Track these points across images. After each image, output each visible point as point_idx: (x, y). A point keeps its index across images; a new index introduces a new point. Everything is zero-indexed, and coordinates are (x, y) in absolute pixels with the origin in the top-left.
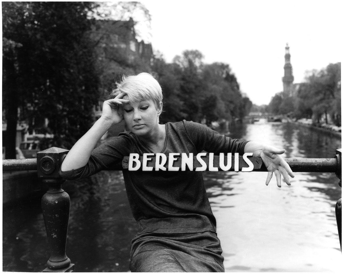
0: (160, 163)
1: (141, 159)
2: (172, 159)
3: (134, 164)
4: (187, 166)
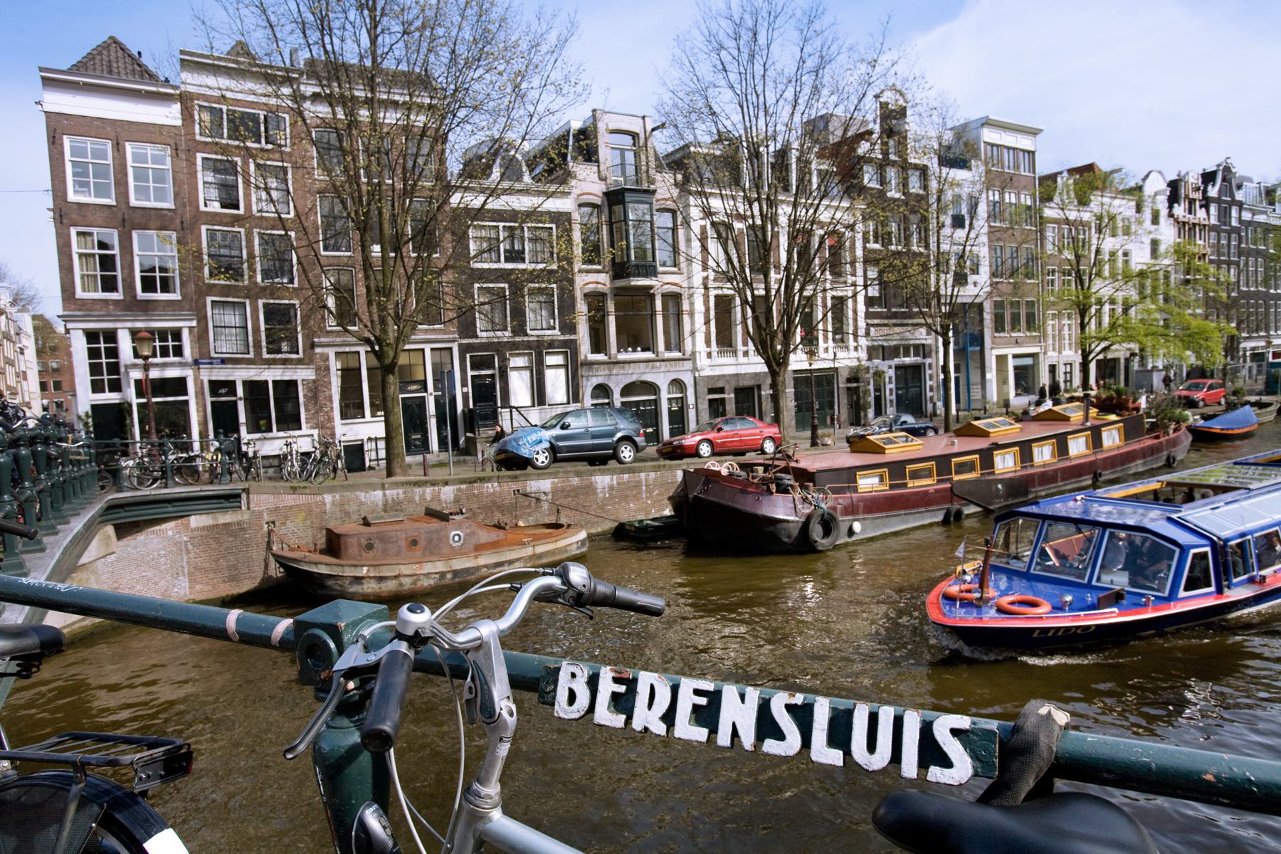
0: (650, 705)
1: (593, 682)
2: (687, 701)
3: (572, 697)
4: (735, 733)
